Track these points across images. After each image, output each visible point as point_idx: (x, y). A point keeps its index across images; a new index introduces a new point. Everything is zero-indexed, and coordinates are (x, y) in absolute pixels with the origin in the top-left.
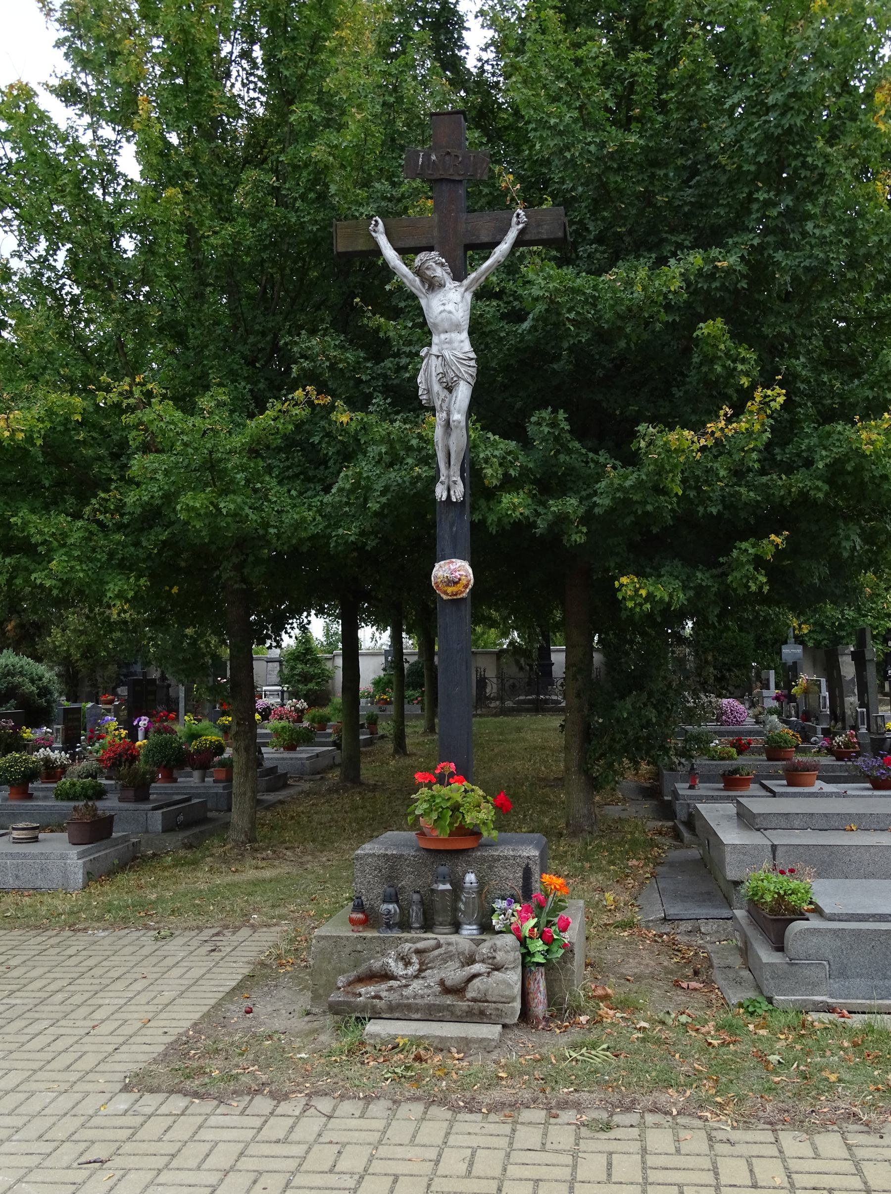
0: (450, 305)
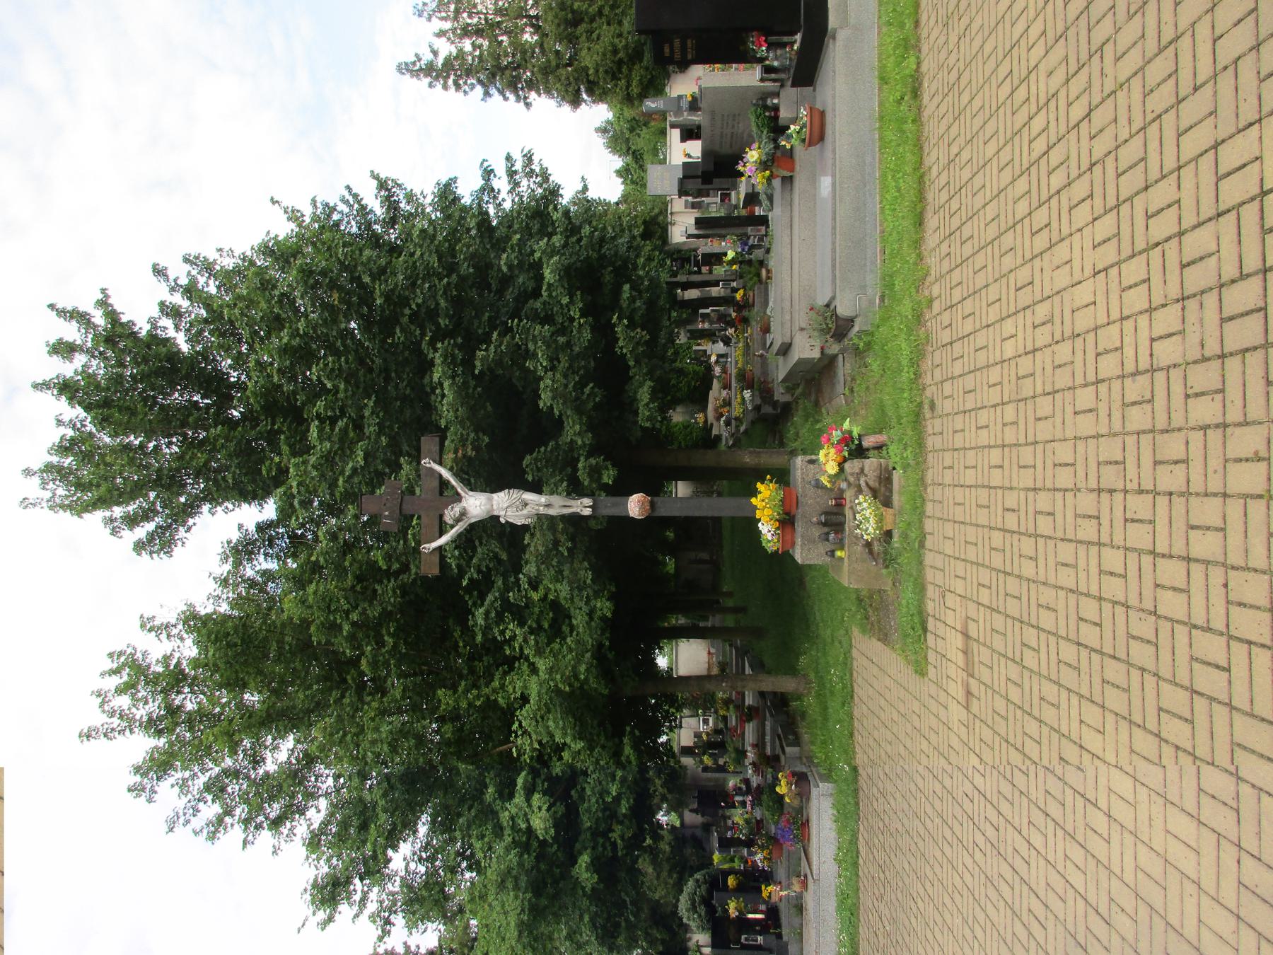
0: (476, 505)
